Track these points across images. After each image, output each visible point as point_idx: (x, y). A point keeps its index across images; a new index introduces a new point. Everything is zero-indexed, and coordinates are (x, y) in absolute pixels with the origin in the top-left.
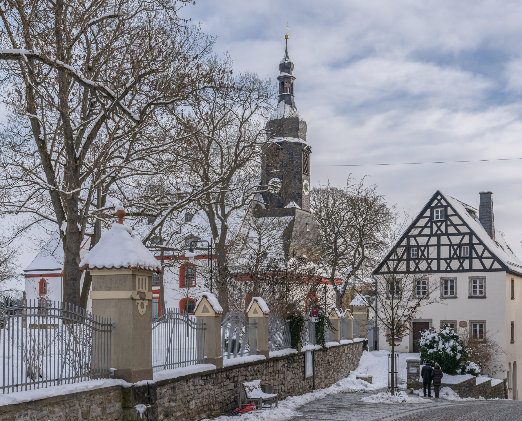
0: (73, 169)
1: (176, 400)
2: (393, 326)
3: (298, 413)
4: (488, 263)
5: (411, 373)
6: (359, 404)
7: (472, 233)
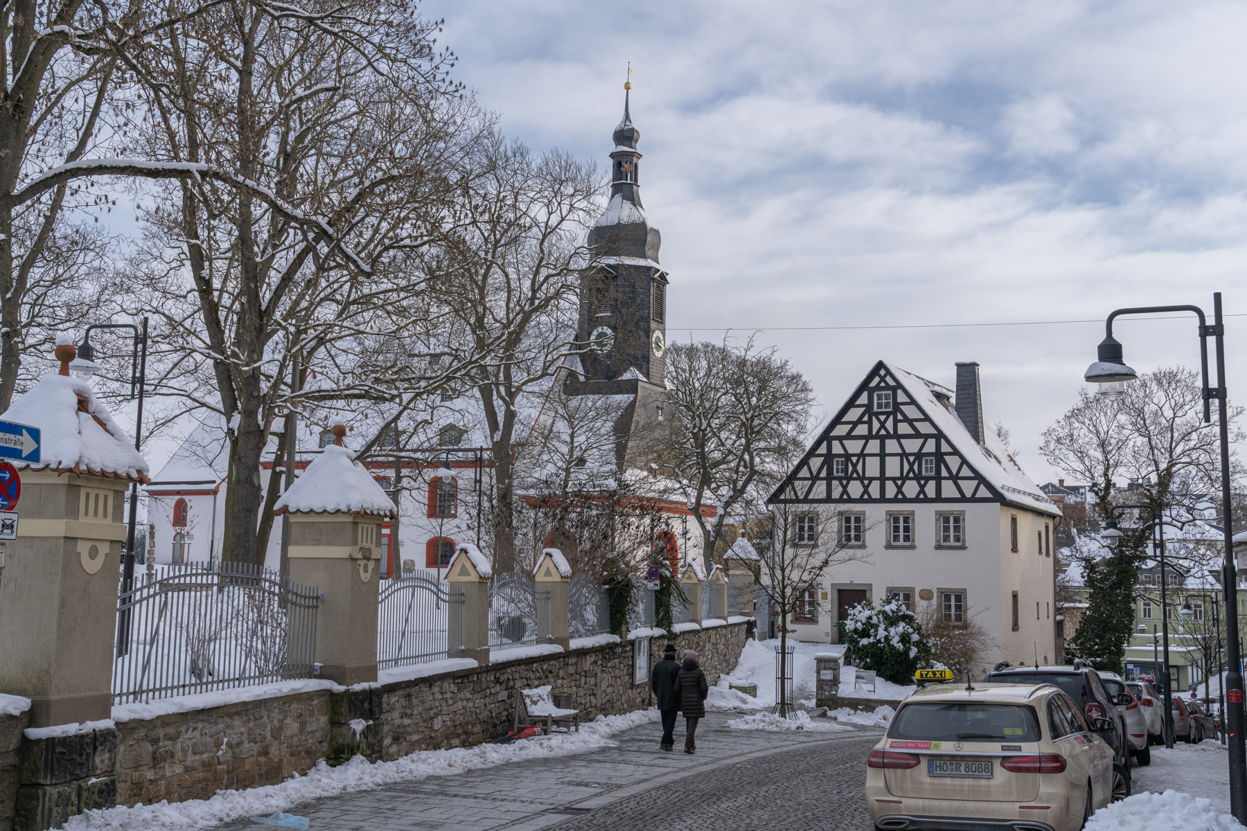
0: (255, 329)
1: (412, 715)
2: (784, 600)
3: (612, 741)
4: (968, 487)
5: (824, 680)
6: (720, 731)
7: (940, 436)
